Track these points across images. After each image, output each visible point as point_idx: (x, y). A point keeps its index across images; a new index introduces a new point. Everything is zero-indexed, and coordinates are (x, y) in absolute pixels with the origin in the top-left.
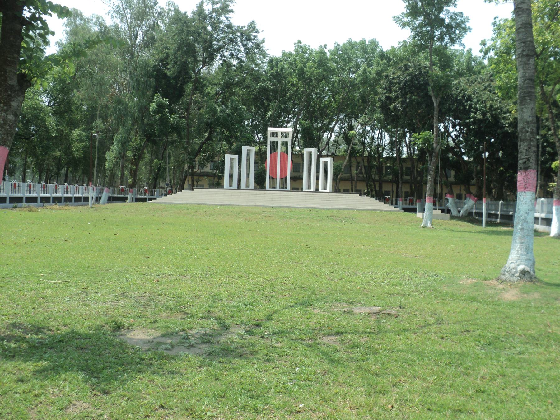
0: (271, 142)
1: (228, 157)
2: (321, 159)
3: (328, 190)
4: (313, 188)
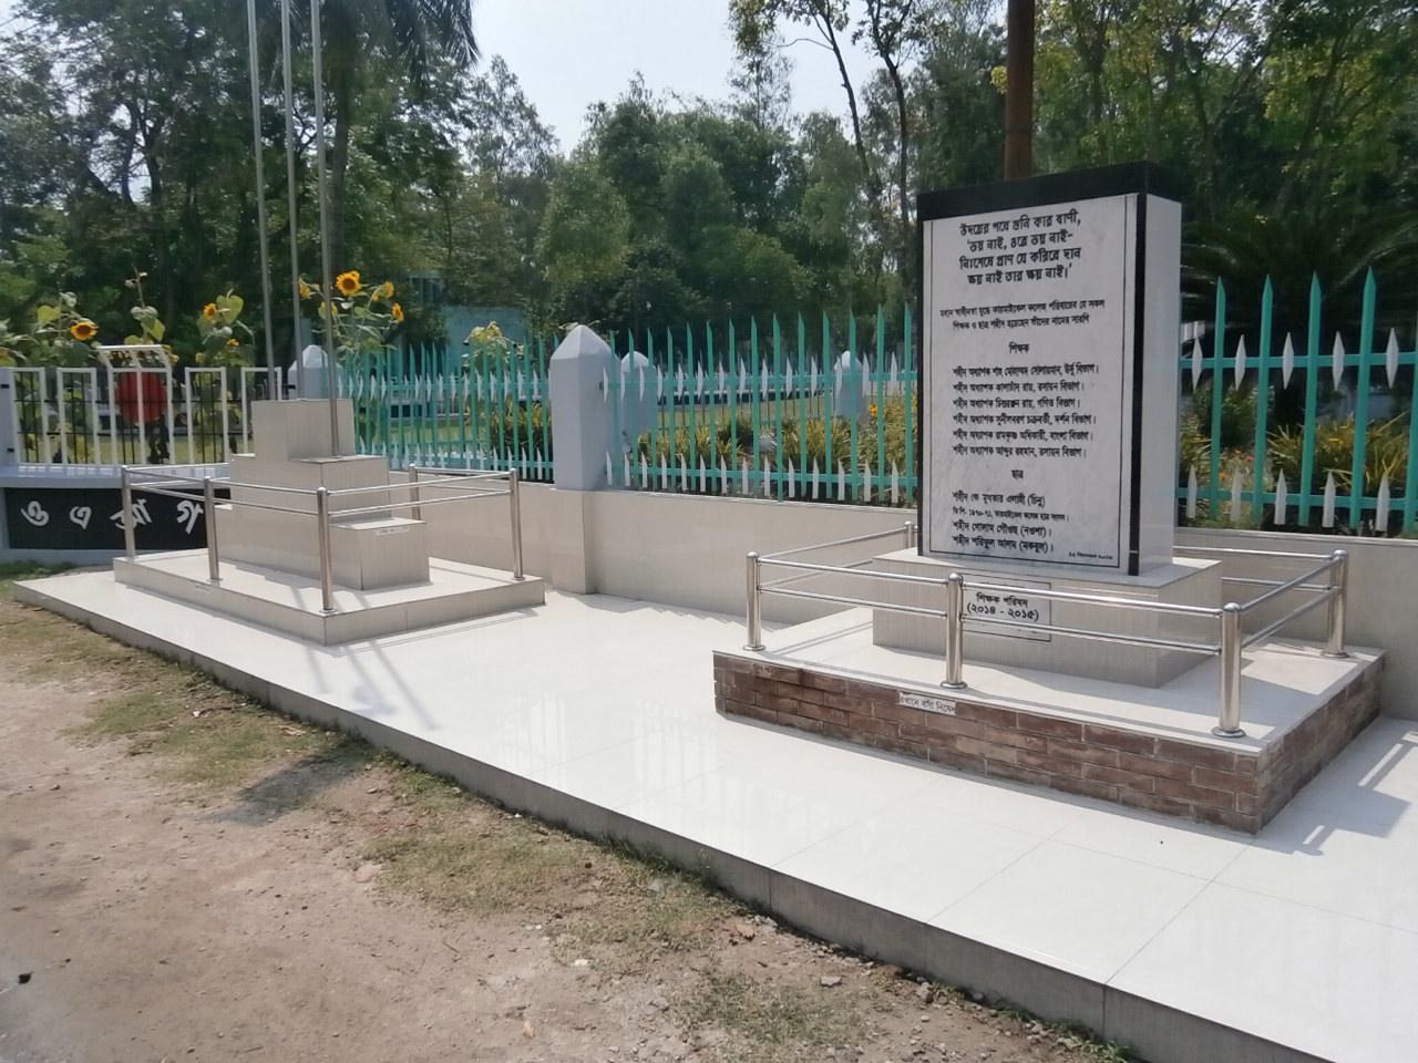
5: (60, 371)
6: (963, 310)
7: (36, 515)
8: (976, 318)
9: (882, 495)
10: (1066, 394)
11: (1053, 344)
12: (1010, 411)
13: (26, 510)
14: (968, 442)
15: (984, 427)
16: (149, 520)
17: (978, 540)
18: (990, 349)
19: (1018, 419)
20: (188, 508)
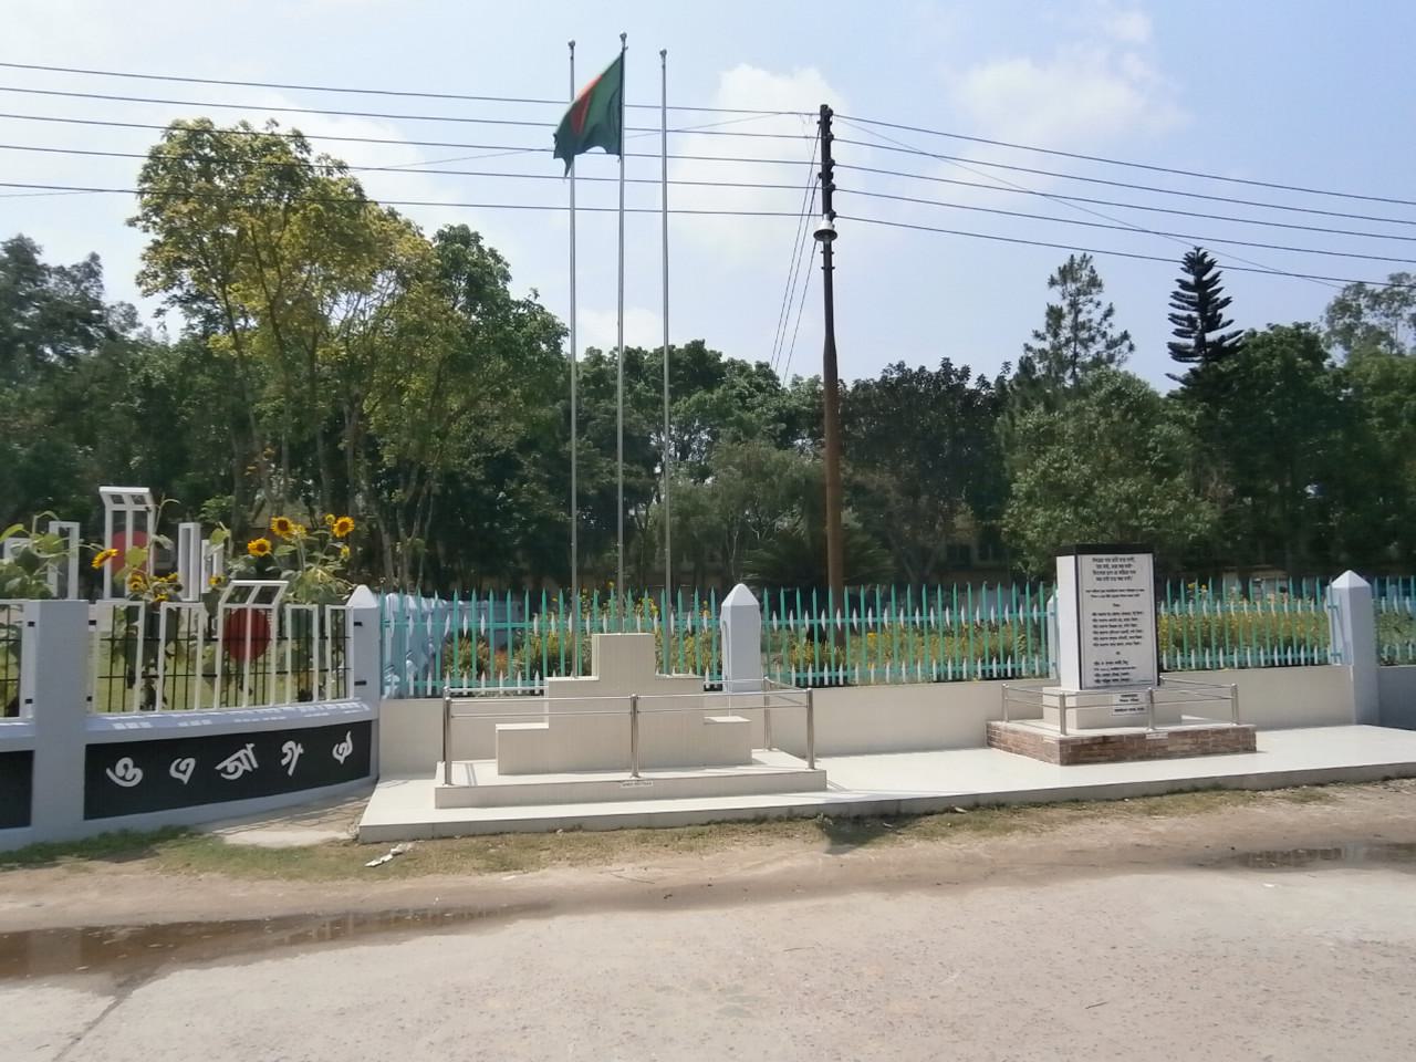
5: (328, 608)
6: (1095, 591)
7: (127, 773)
8: (1099, 594)
9: (958, 677)
10: (1134, 622)
11: (1128, 605)
12: (1115, 629)
13: (114, 771)
14: (1100, 642)
15: (1105, 635)
16: (255, 766)
17: (1105, 681)
18: (1106, 605)
19: (1117, 632)
20: (291, 749)
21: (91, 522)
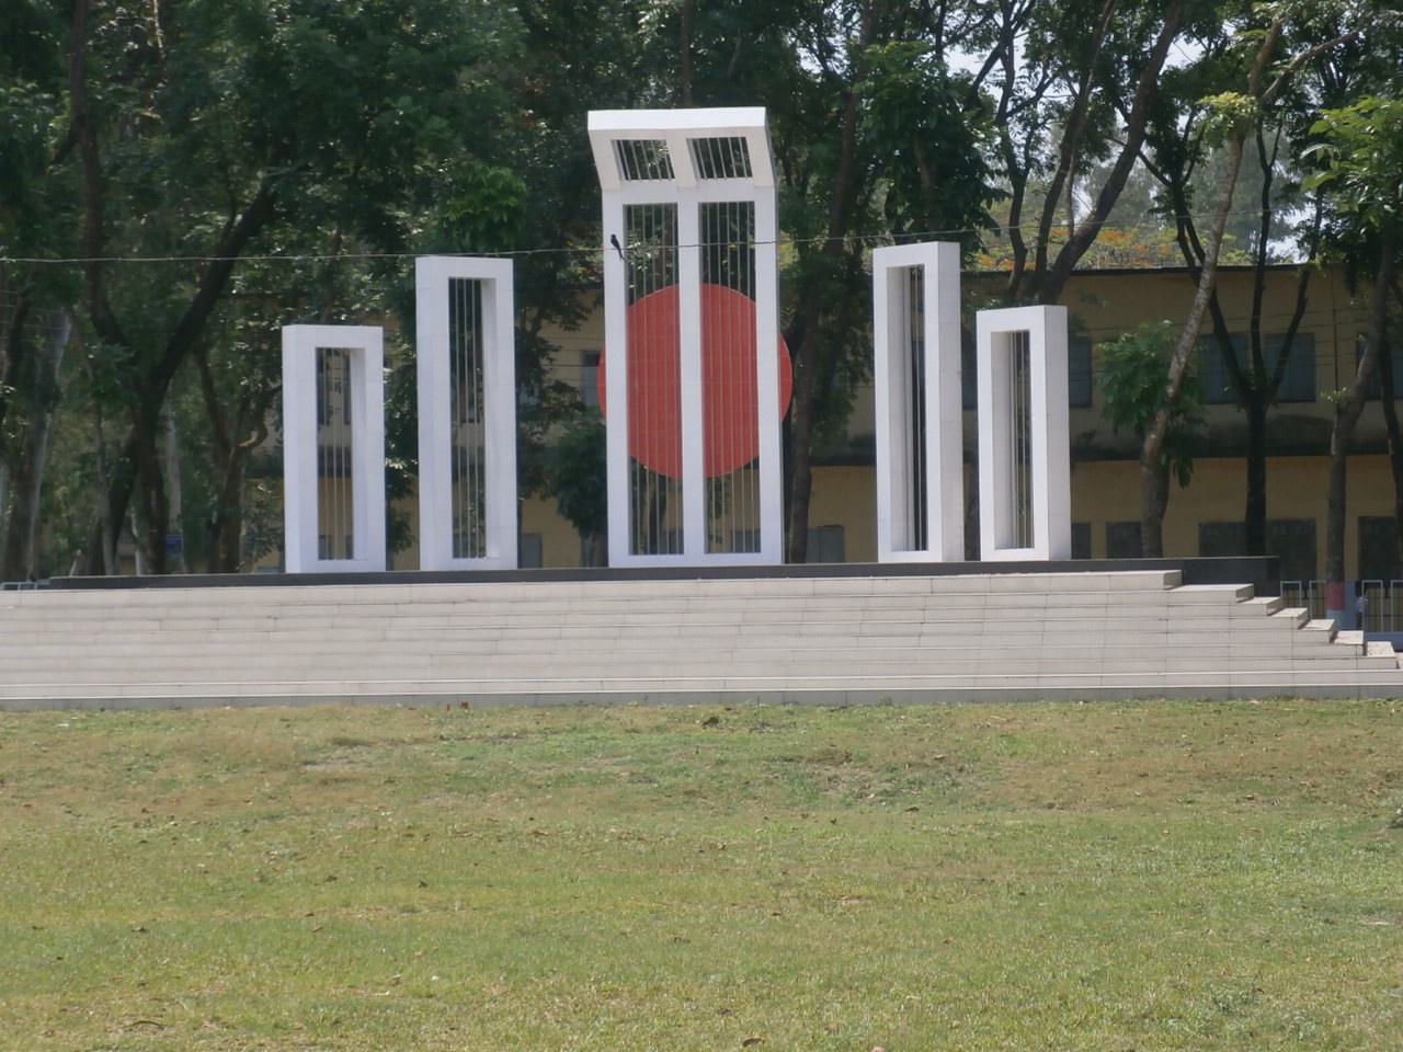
0: (633, 214)
1: (300, 344)
2: (983, 317)
3: (1040, 551)
4: (942, 543)
21: (546, 226)
